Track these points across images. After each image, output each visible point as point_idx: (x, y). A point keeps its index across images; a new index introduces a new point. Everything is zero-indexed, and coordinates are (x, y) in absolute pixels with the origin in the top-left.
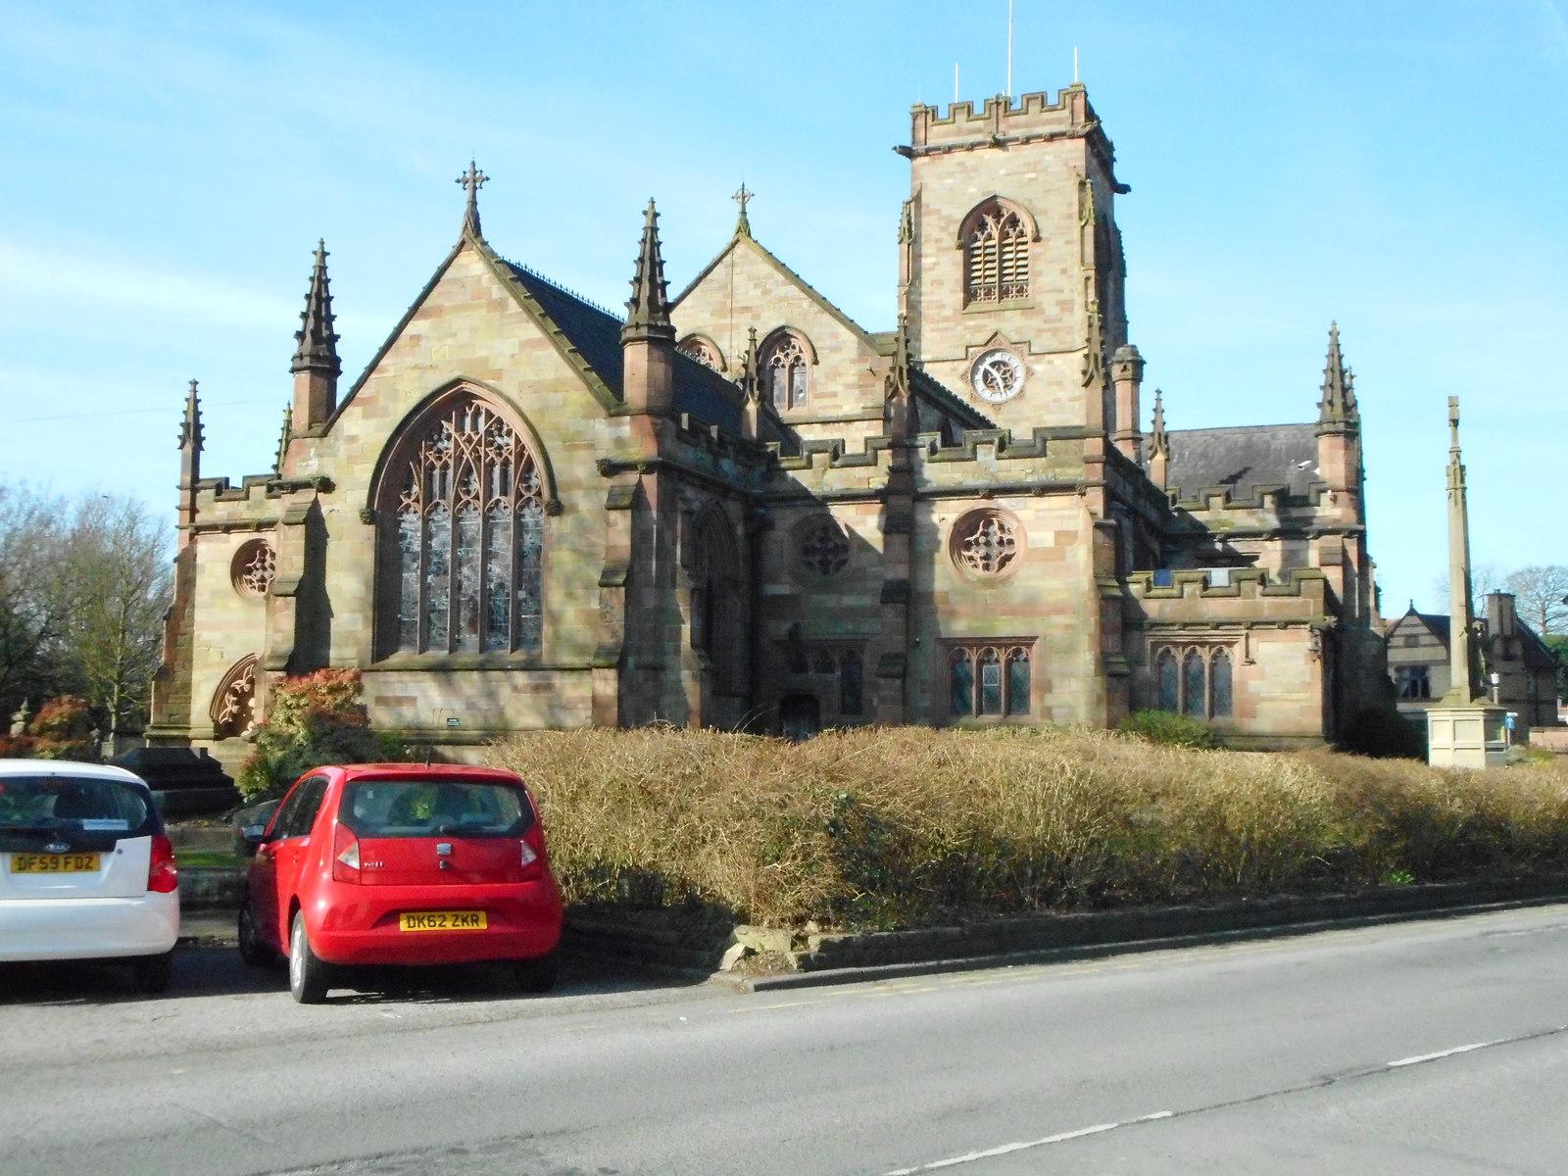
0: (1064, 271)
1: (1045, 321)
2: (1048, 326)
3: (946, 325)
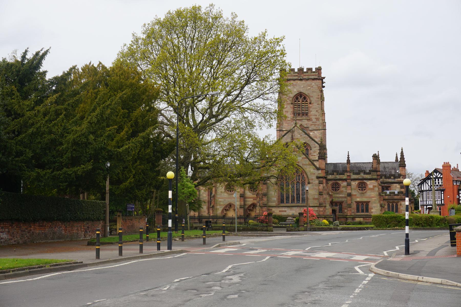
0: (317, 111)
1: (313, 123)
2: (313, 124)
3: (289, 122)
